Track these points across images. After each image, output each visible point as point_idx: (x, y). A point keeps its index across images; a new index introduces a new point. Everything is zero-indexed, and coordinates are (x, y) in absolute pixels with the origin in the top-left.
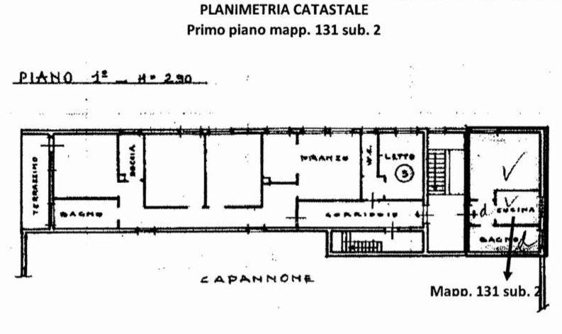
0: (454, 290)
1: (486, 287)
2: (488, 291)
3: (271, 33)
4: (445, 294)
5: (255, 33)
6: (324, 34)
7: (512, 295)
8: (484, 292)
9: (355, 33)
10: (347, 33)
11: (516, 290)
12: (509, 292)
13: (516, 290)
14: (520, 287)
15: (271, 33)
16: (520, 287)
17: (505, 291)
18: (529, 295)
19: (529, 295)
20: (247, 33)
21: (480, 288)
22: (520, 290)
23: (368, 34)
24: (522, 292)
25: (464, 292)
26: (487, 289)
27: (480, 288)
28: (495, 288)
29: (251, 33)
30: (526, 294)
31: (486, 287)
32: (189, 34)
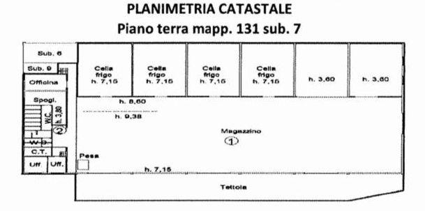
0: (214, 28)
1: (246, 25)
2: (249, 28)
3: (194, 32)
4: (168, 29)
5: (143, 32)
6: (246, 33)
7: (143, 27)
8: (244, 29)
9: (275, 32)
10: (268, 31)
11: (276, 27)
12: (269, 29)
13: (276, 27)
14: (280, 24)
15: (194, 32)
16: (280, 24)
17: (265, 28)
18: (231, 32)
19: (231, 32)
20: (135, 32)
21: (240, 25)
22: (280, 28)
23: (288, 32)
24: (282, 30)
25: (149, 30)
26: (247, 26)
27: (240, 25)
28: (256, 25)
29: (139, 32)
30: (286, 31)
31: (246, 25)
32: (119, 32)
